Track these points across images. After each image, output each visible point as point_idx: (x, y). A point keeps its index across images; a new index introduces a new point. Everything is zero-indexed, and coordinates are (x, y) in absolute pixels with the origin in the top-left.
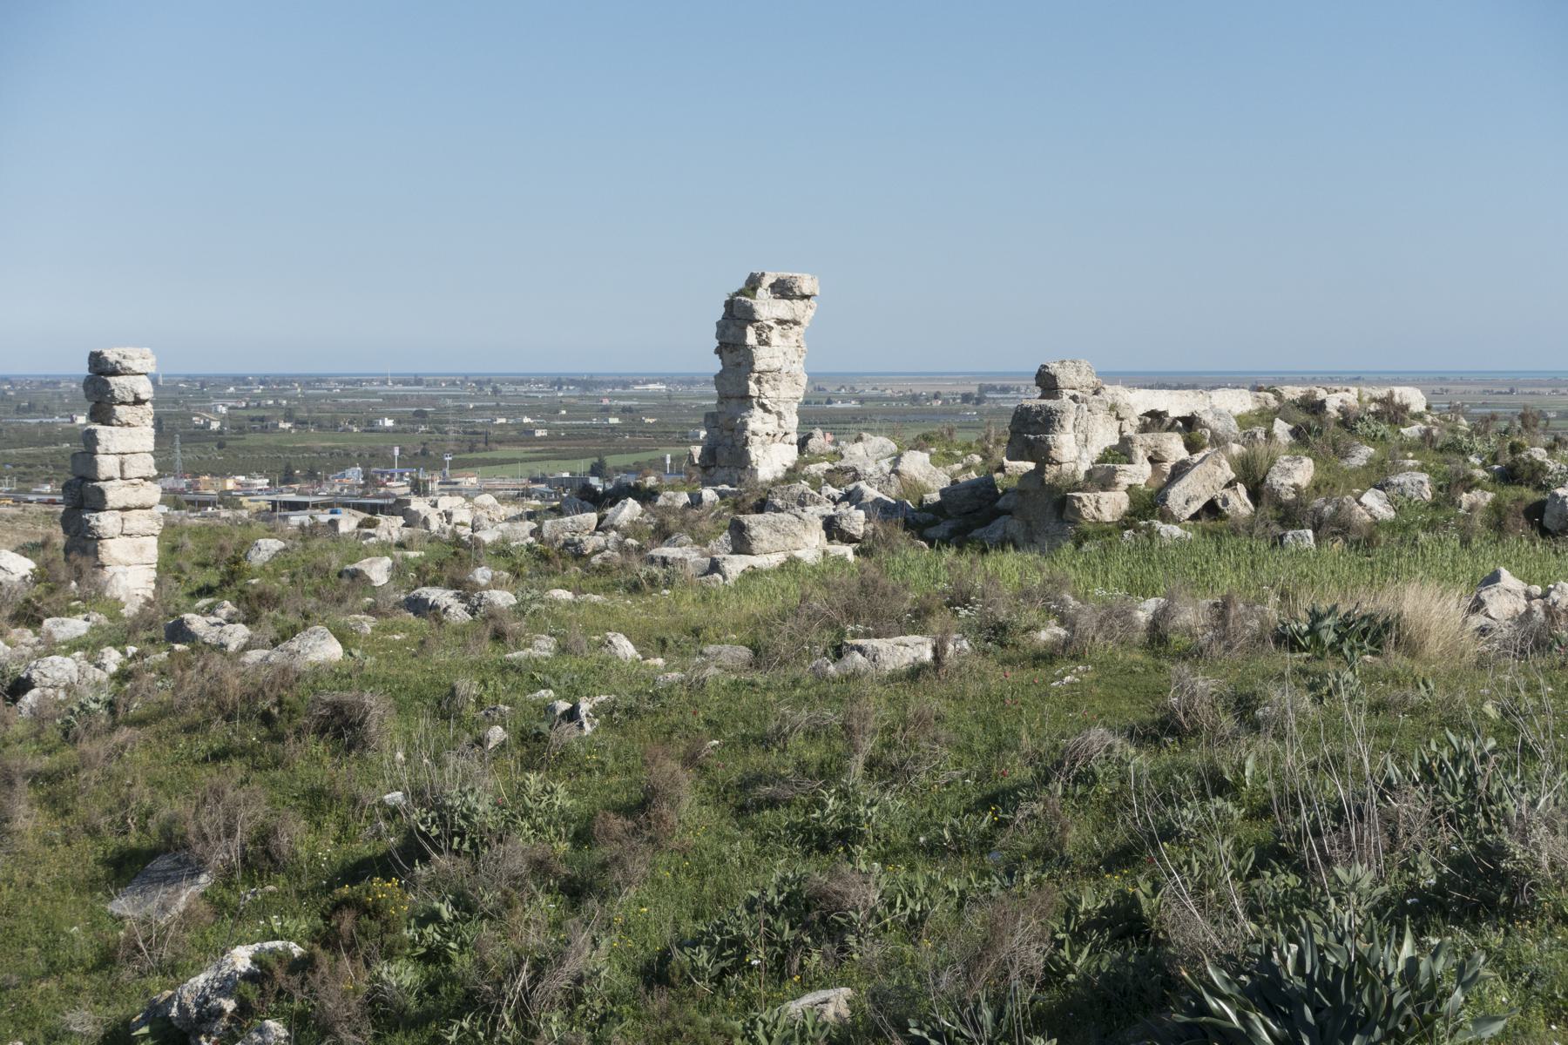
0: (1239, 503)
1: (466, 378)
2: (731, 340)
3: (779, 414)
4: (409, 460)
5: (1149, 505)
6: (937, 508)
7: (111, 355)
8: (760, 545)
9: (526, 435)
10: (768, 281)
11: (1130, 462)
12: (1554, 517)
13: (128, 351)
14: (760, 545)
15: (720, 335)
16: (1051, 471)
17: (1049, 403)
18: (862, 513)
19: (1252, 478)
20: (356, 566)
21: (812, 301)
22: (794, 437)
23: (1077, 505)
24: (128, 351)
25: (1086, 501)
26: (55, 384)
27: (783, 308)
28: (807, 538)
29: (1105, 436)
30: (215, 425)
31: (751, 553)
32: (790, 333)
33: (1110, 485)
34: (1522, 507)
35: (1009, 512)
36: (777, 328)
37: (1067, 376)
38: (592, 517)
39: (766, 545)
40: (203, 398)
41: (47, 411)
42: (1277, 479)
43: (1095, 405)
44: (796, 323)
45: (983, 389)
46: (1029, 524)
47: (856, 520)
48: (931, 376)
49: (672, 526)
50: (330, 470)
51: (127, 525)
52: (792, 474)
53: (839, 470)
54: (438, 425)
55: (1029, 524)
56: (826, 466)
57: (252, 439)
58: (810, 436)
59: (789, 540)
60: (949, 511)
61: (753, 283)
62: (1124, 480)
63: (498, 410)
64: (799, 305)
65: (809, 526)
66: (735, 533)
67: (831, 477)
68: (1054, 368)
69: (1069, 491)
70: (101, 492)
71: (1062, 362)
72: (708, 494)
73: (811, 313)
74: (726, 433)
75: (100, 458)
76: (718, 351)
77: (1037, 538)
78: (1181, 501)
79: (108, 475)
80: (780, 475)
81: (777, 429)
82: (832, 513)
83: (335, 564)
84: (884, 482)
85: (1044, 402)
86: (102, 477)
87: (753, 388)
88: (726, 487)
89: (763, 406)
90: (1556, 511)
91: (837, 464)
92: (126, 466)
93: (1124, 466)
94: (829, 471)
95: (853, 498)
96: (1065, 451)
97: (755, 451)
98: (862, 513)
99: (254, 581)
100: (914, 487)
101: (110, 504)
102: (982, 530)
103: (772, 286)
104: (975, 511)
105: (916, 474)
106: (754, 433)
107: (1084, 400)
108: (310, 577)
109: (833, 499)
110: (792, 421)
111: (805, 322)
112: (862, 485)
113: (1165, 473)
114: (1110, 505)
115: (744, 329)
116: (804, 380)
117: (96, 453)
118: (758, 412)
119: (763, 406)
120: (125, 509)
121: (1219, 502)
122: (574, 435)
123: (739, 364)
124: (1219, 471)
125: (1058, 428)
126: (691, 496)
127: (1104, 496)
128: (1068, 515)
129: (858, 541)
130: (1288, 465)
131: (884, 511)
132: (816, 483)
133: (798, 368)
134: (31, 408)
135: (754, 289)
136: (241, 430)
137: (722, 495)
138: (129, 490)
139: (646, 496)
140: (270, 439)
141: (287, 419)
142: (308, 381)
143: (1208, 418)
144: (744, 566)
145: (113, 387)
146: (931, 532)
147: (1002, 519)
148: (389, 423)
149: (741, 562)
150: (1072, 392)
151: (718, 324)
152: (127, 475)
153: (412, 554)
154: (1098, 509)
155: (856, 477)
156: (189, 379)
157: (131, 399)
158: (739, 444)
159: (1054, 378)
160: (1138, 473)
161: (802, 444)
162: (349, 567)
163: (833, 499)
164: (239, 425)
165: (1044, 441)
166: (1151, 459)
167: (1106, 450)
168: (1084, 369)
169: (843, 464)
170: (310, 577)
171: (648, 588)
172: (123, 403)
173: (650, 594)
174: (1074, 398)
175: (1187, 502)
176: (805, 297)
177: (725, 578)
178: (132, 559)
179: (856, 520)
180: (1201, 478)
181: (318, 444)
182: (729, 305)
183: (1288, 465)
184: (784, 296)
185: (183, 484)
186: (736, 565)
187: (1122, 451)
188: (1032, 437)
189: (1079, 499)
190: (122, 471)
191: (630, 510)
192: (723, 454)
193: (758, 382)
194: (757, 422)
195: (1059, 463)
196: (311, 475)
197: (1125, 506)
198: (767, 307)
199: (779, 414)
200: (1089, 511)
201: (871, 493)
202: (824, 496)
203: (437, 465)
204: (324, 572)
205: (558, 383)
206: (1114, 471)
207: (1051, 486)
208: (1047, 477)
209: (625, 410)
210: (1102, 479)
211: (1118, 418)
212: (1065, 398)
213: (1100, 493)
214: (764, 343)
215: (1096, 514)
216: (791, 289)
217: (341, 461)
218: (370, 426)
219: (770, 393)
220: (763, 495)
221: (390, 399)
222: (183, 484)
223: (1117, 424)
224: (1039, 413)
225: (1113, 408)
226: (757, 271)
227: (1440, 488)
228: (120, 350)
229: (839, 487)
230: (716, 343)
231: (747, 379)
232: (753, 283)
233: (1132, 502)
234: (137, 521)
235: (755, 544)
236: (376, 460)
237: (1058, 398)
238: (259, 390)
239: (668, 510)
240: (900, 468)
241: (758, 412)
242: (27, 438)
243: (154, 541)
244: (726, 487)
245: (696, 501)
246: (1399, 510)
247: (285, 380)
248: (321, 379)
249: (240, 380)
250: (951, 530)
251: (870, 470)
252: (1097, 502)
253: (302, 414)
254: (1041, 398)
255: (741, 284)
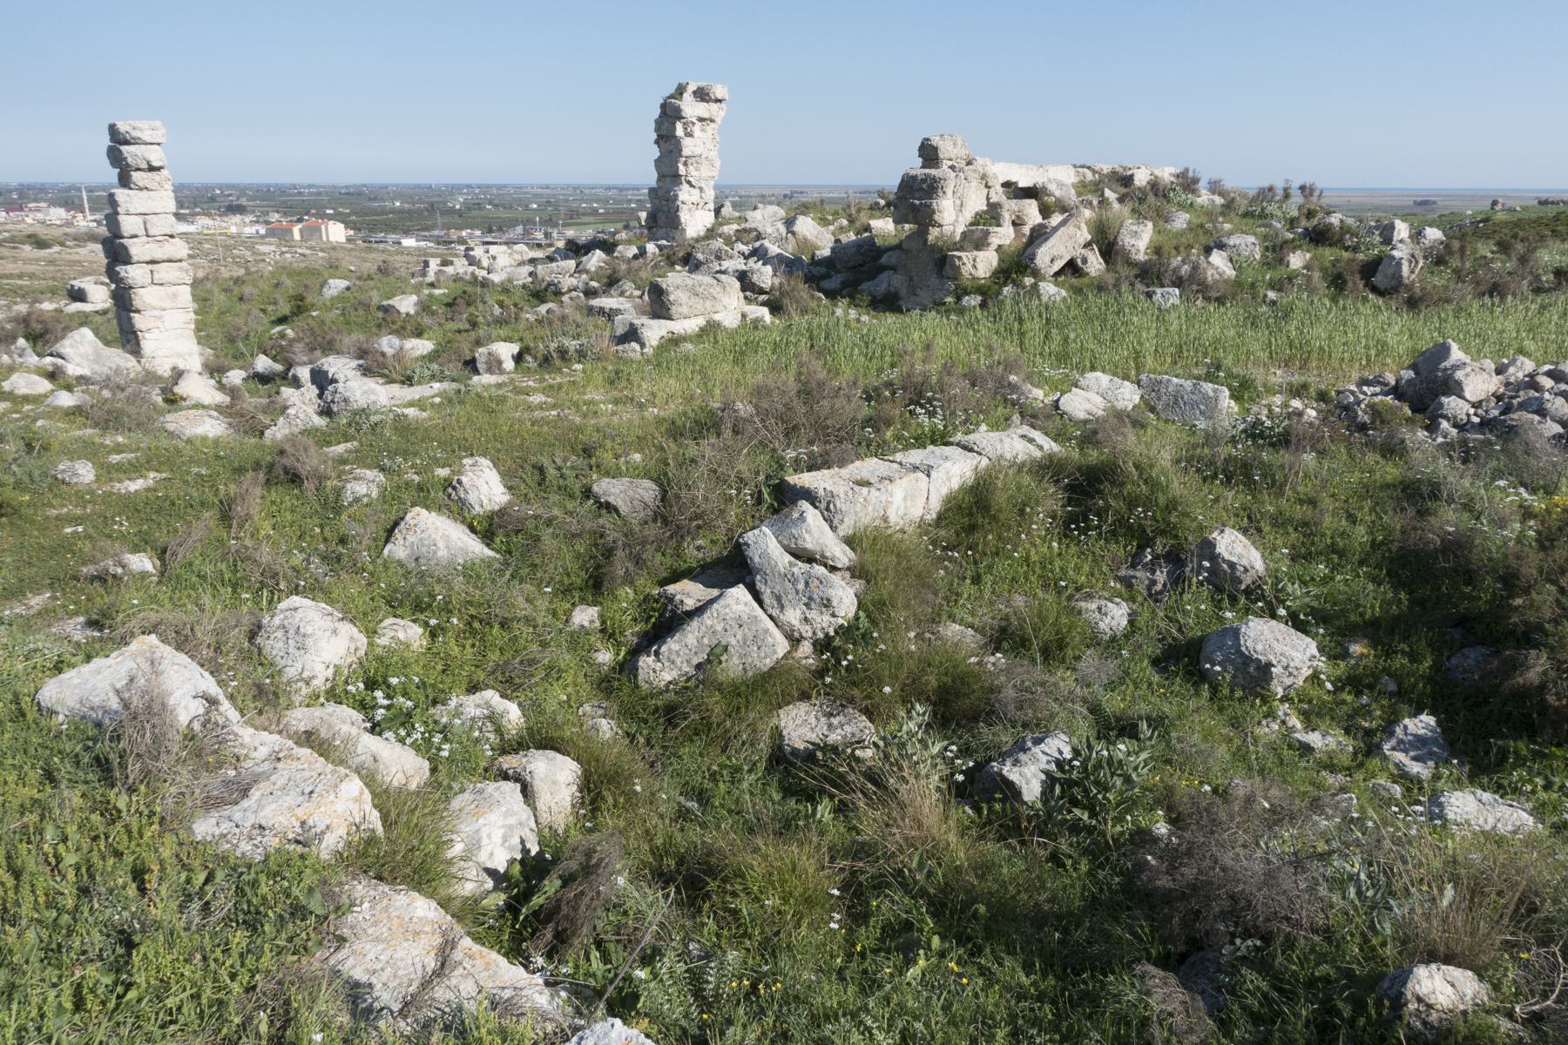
0: (1095, 264)
1: (568, 186)
2: (665, 132)
3: (701, 189)
4: (543, 223)
5: (1017, 266)
6: (828, 262)
7: (123, 127)
8: (679, 310)
9: (595, 212)
10: (692, 88)
11: (999, 225)
12: (1386, 276)
13: (138, 124)
14: (679, 310)
15: (657, 130)
16: (934, 233)
17: (933, 172)
18: (769, 269)
19: (1107, 244)
20: (390, 302)
21: (723, 105)
22: (711, 206)
23: (957, 263)
24: (138, 124)
25: (965, 260)
26: (386, 187)
27: (701, 109)
28: (726, 300)
29: (976, 203)
30: (458, 207)
31: (670, 318)
32: (708, 128)
33: (983, 245)
34: (1356, 268)
35: (893, 268)
36: (698, 124)
37: (947, 149)
38: (572, 263)
39: (685, 310)
40: (452, 194)
41: (383, 200)
42: (1126, 240)
43: (970, 175)
44: (712, 121)
45: (792, 192)
46: (911, 279)
47: (765, 276)
48: (770, 187)
49: (621, 273)
50: (509, 227)
51: (156, 276)
52: (711, 233)
53: (745, 230)
54: (556, 208)
55: (911, 279)
56: (735, 227)
57: (475, 213)
58: (722, 206)
59: (708, 304)
60: (838, 266)
61: (680, 91)
62: (995, 241)
63: (583, 200)
64: (714, 106)
65: (728, 289)
66: (653, 296)
67: (741, 235)
68: (936, 141)
69: (949, 250)
70: (126, 248)
71: (942, 136)
72: (651, 248)
73: (722, 114)
74: (664, 203)
75: (121, 218)
76: (657, 142)
77: (918, 291)
78: (1047, 260)
79: (133, 233)
80: (702, 233)
81: (699, 200)
82: (744, 268)
83: (375, 301)
84: (780, 240)
85: (927, 171)
86: (125, 234)
87: (682, 170)
88: (664, 242)
89: (689, 183)
90: (1390, 271)
91: (743, 226)
92: (148, 226)
93: (996, 229)
94: (738, 231)
95: (759, 254)
96: (946, 215)
97: (684, 216)
98: (769, 269)
99: (314, 314)
100: (804, 244)
101: (135, 258)
102: (869, 283)
103: (694, 93)
104: (861, 265)
105: (808, 234)
106: (683, 203)
107: (961, 170)
108: (356, 310)
109: (743, 254)
110: (710, 195)
111: (718, 120)
112: (766, 243)
113: (1024, 235)
114: (981, 264)
115: (674, 124)
116: (718, 164)
117: (117, 214)
118: (685, 187)
119: (689, 183)
120: (153, 262)
121: (1079, 261)
122: (616, 212)
123: (671, 151)
124: (1079, 233)
125: (941, 194)
126: (638, 248)
127: (981, 255)
128: (948, 271)
129: (766, 293)
130: (1135, 228)
131: (787, 265)
132: (729, 241)
133: (713, 154)
134: (375, 199)
135: (681, 94)
136: (469, 209)
137: (660, 248)
138: (154, 246)
139: (608, 247)
140: (483, 213)
141: (490, 204)
142: (500, 187)
143: (1052, 187)
144: (664, 333)
145: (126, 155)
146: (826, 284)
147: (886, 274)
148: (535, 206)
149: (660, 329)
150: (950, 163)
151: (656, 121)
152: (151, 232)
153: (437, 292)
154: (974, 267)
155: (759, 237)
156: (446, 186)
157: (145, 166)
158: (672, 211)
159: (935, 149)
160: (1004, 235)
161: (717, 211)
162: (385, 303)
163: (743, 254)
164: (468, 207)
165: (929, 206)
166: (1014, 224)
167: (977, 214)
168: (959, 142)
169: (748, 226)
170: (356, 310)
171: (558, 362)
172: (138, 169)
173: (560, 370)
174: (952, 168)
175: (1052, 261)
176: (718, 101)
177: (643, 345)
178: (166, 304)
179: (765, 276)
180: (1064, 239)
181: (503, 216)
182: (663, 106)
183: (1135, 228)
184: (703, 100)
185: (442, 233)
186: (654, 331)
187: (992, 214)
188: (917, 202)
189: (960, 258)
190: (146, 230)
191: (596, 259)
192: (662, 219)
193: (685, 164)
194: (685, 194)
195: (940, 226)
196: (500, 229)
197: (995, 263)
198: (691, 108)
199: (701, 189)
200: (967, 270)
201: (774, 250)
202: (735, 252)
203: (556, 225)
204: (367, 307)
205: (609, 188)
206: (987, 233)
207: (933, 246)
208: (930, 238)
209: (639, 201)
210: (975, 239)
211: (987, 186)
212: (945, 167)
213: (976, 253)
214: (689, 135)
215: (973, 272)
216: (708, 94)
217: (513, 223)
218: (526, 208)
219: (694, 173)
220: (689, 250)
221: (535, 195)
222: (442, 233)
223: (986, 191)
224: (924, 181)
225: (984, 177)
226: (683, 81)
227: (1267, 249)
228: (132, 123)
229: (746, 244)
230: (655, 136)
231: (677, 162)
232: (680, 91)
233: (1001, 260)
234: (165, 272)
235: (674, 309)
236: (528, 222)
237: (938, 167)
238: (477, 191)
239: (622, 258)
240: (795, 229)
241: (685, 187)
242: (375, 212)
243: (188, 289)
244: (664, 242)
245: (642, 252)
246: (1239, 269)
247: (488, 187)
248: (505, 186)
249: (469, 186)
250: (842, 283)
251: (769, 230)
252: (974, 260)
253: (496, 202)
254: (923, 167)
255: (672, 90)
